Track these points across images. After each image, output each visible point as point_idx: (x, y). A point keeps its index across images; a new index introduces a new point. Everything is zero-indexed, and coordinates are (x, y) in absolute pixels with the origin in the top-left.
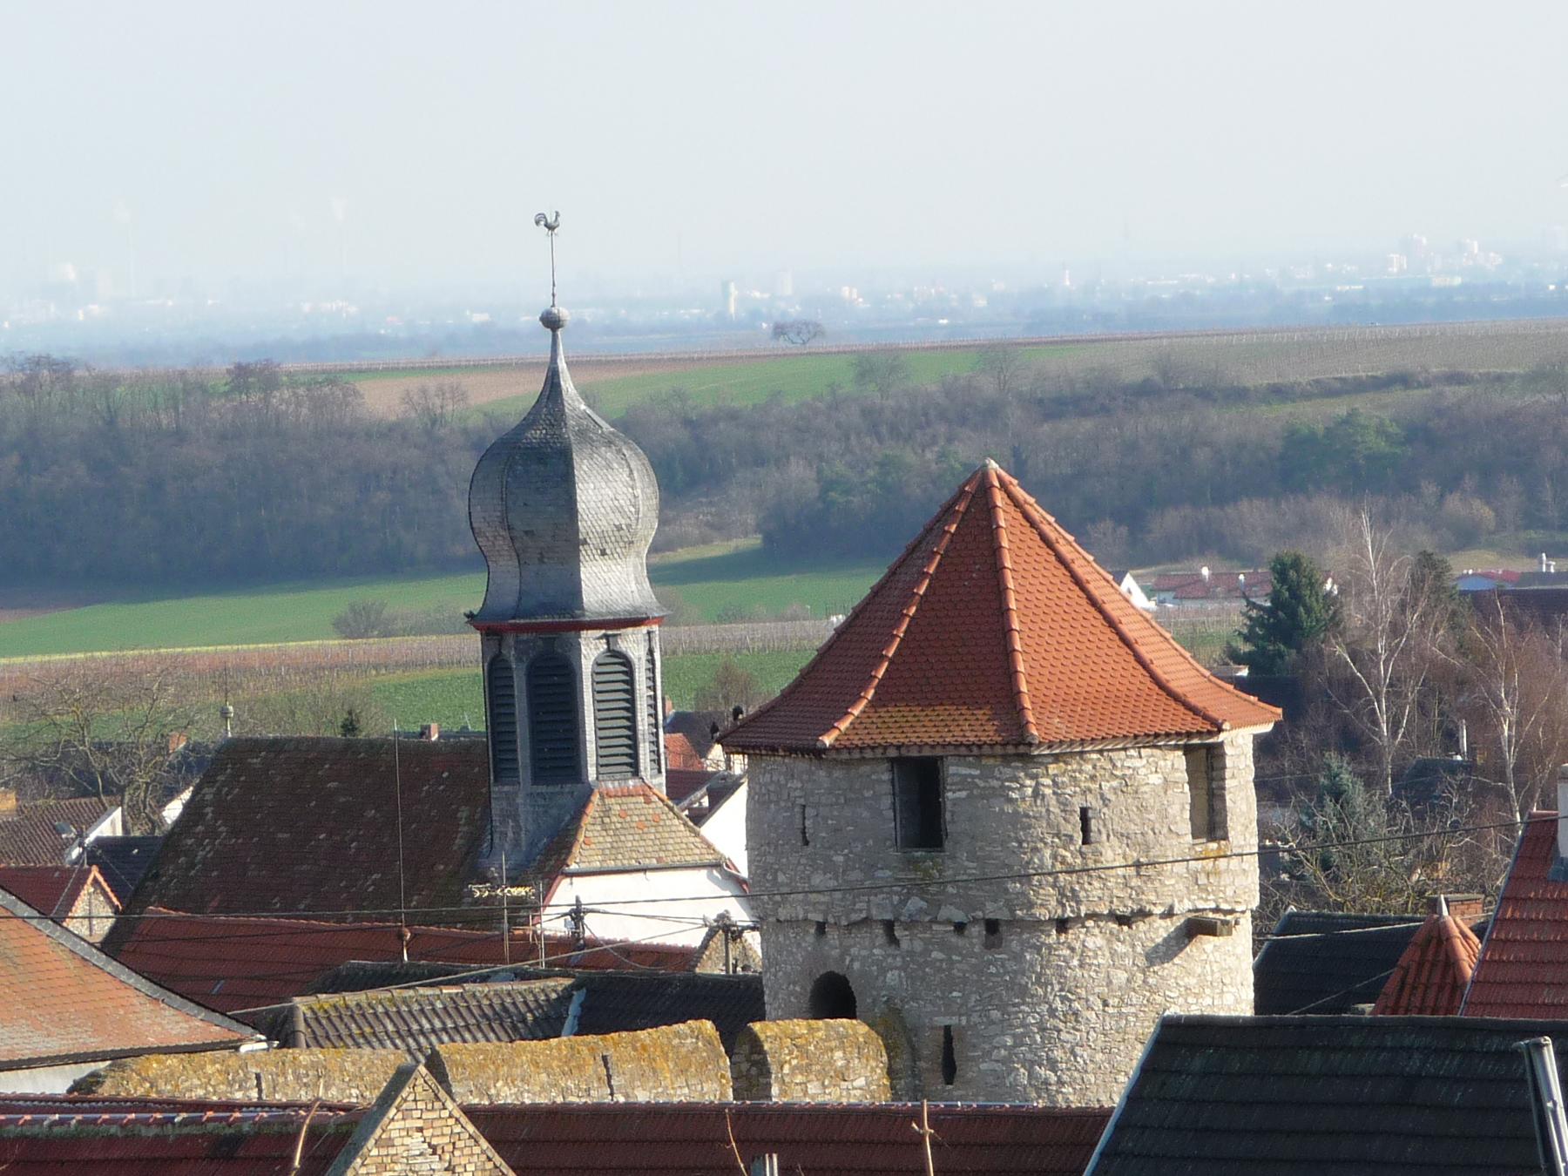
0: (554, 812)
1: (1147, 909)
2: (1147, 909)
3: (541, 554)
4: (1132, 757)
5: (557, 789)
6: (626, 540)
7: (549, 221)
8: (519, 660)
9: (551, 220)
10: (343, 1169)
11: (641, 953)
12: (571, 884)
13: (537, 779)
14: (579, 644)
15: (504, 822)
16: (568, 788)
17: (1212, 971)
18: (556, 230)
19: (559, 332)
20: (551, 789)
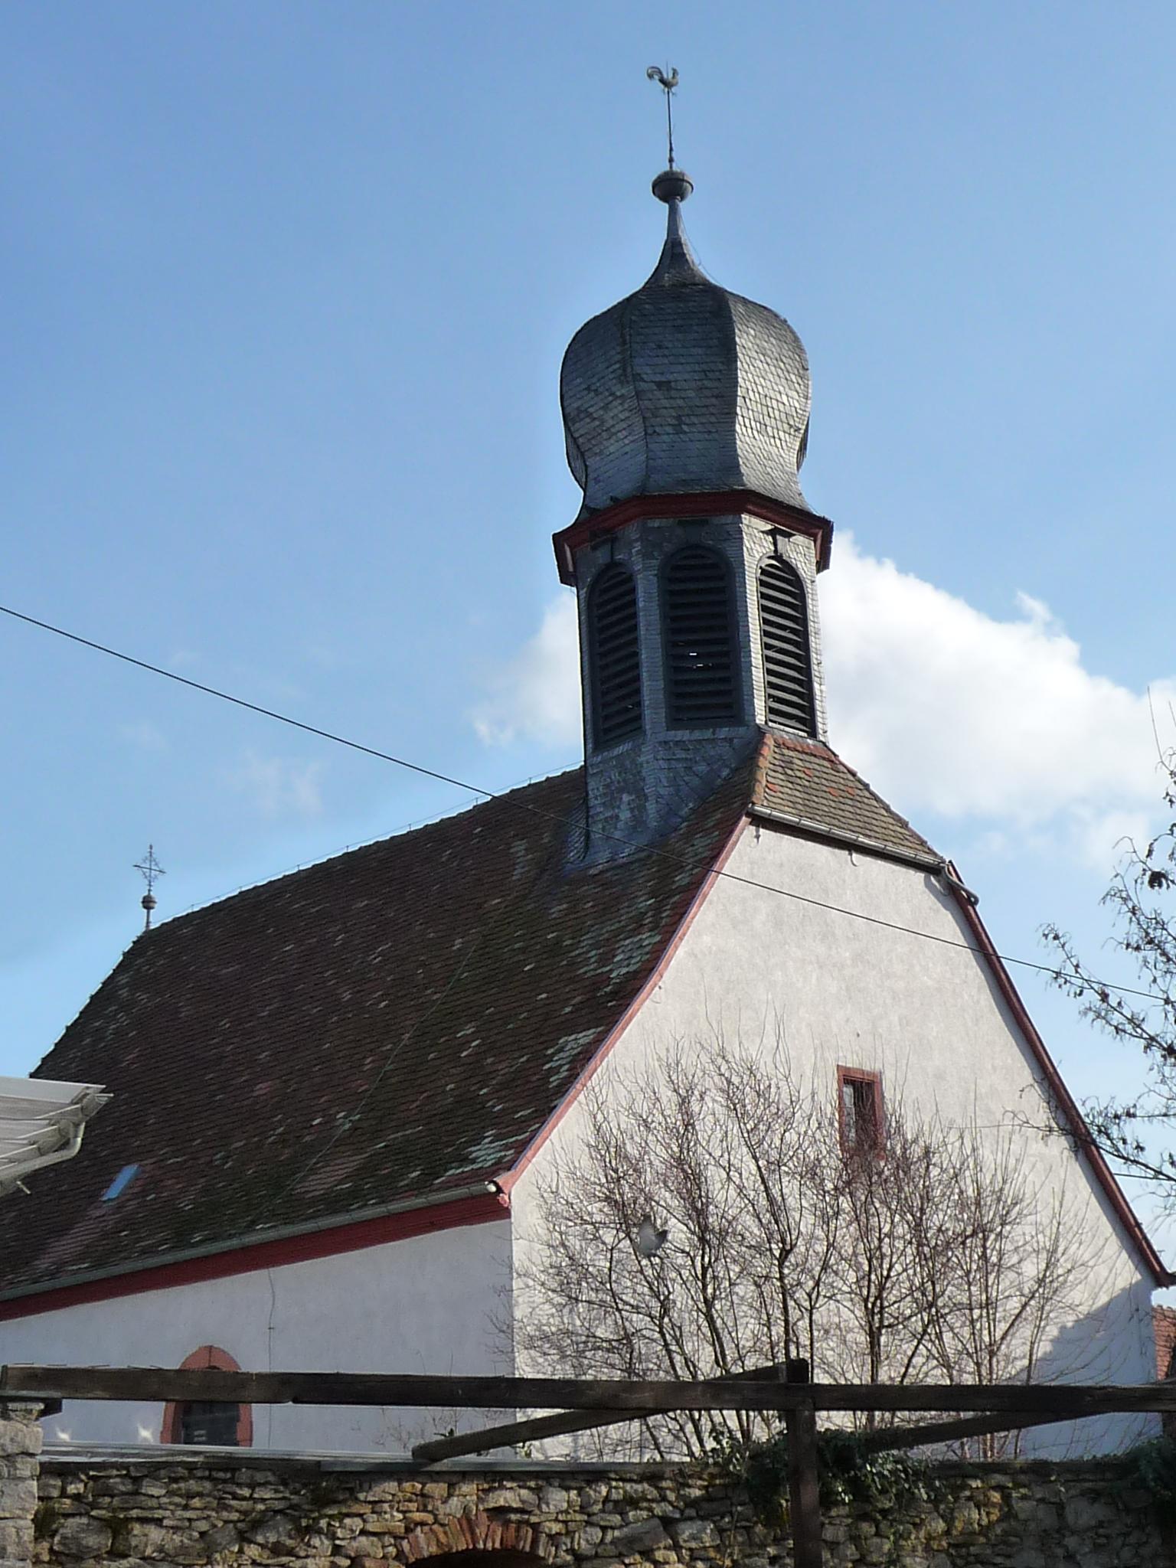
0: (702, 768)
1: (218, 1541)
2: (218, 1541)
3: (679, 417)
4: (796, 1179)
5: (708, 734)
6: (792, 423)
7: (665, 76)
8: (646, 555)
9: (668, 75)
10: (123, 979)
11: (438, 1382)
12: (758, 837)
13: (675, 720)
14: (741, 532)
15: (611, 799)
16: (724, 732)
17: (869, 1287)
18: (673, 89)
19: (683, 206)
20: (697, 735)
